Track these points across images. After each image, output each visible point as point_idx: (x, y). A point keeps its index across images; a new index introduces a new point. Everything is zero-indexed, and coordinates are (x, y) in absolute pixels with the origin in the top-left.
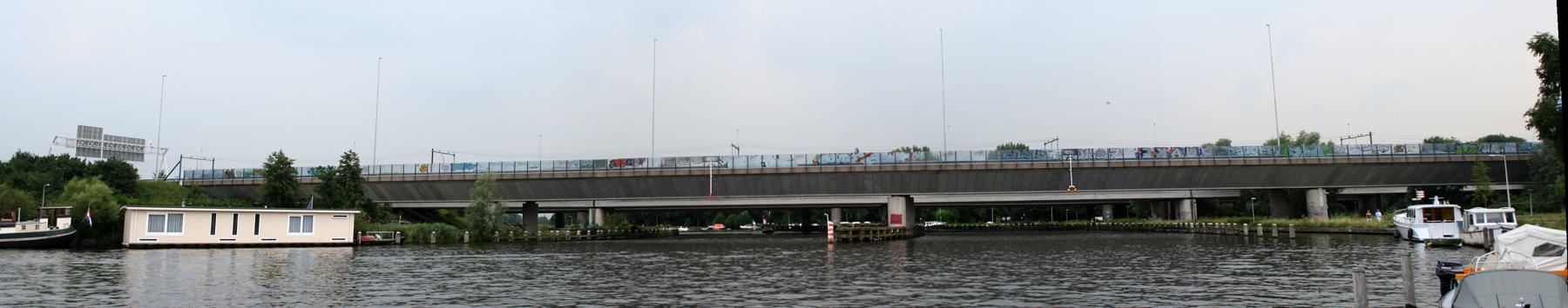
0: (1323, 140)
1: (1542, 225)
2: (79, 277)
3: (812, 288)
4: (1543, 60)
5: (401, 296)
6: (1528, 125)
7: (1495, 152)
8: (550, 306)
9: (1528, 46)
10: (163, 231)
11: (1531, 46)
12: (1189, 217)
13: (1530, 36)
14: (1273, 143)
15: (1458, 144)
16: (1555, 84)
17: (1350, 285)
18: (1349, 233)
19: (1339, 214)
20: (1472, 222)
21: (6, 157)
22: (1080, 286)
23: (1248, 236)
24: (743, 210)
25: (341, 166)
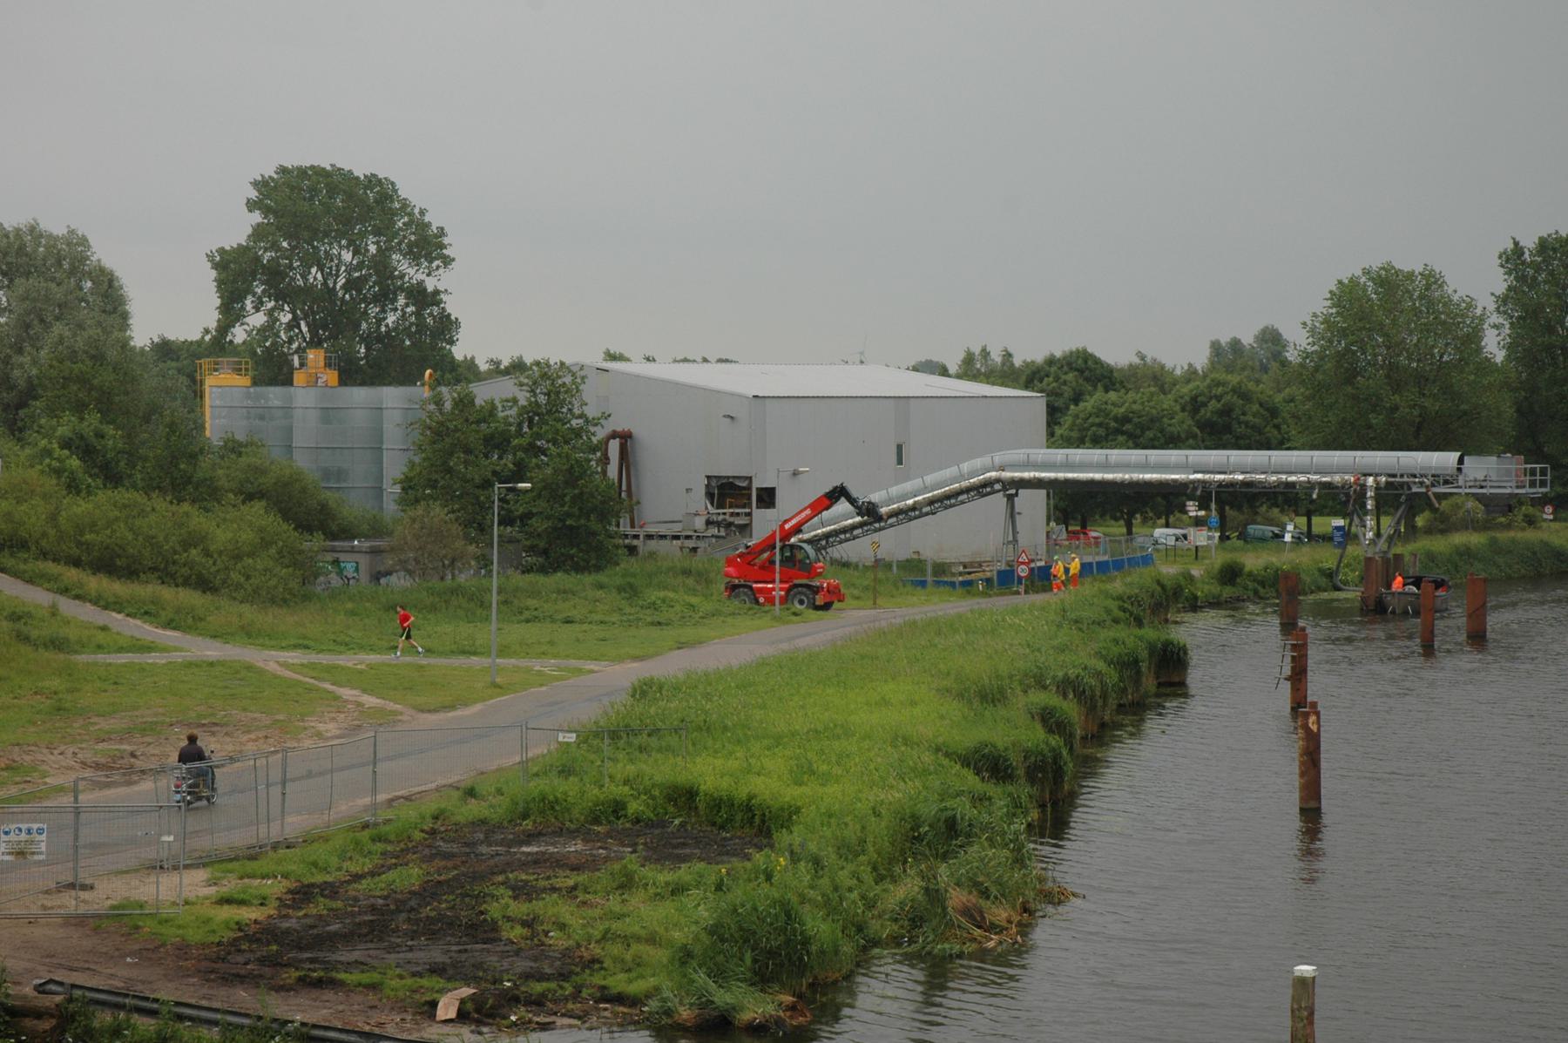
0: (528, 360)
1: (1102, 448)
2: (296, 905)
3: (154, 755)
4: (357, 178)
5: (1502, 893)
6: (492, 361)
7: (689, 633)
8: (665, 1027)
9: (1350, 276)
10: (1097, 563)
11: (210, 257)
12: (88, 537)
13: (205, 326)
14: (219, 287)
15: (349, 177)
16: (784, 1033)
17: (635, 542)
18: (181, 881)
19: (1102, 515)
20: (18, 456)
21: (13, 219)
22: (674, 841)
23: (1309, 515)
24: (820, 540)
25: (1302, 365)
